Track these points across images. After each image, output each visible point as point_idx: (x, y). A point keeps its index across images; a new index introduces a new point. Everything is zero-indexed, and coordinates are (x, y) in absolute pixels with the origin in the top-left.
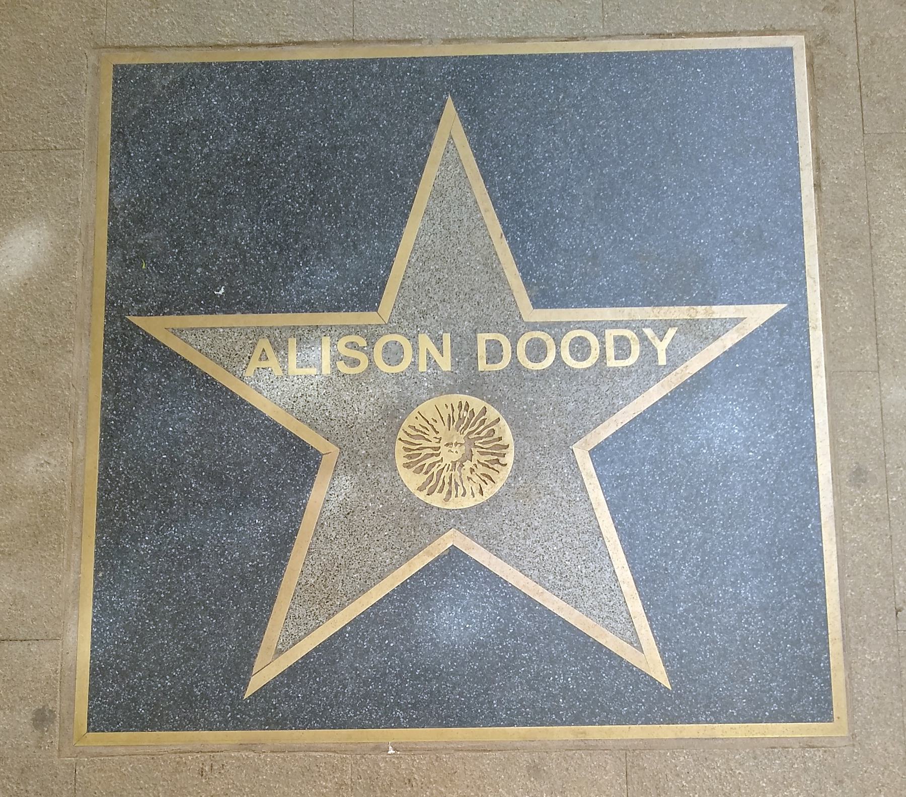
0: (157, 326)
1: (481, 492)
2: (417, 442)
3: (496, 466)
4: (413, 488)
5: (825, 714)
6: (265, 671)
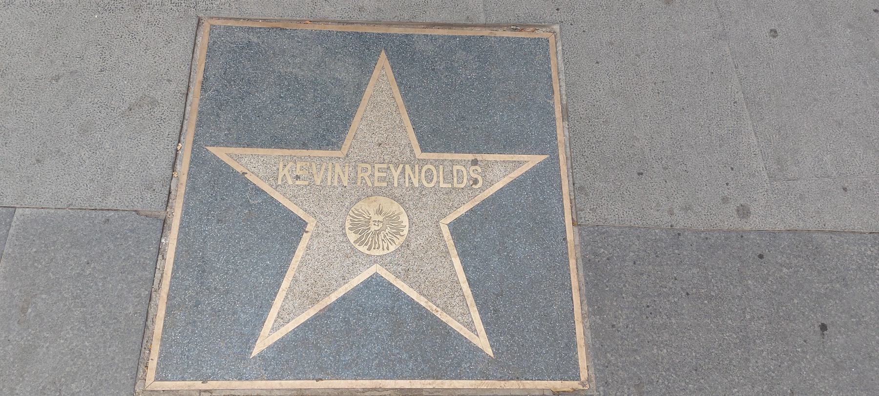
0: (221, 153)
6: (269, 336)
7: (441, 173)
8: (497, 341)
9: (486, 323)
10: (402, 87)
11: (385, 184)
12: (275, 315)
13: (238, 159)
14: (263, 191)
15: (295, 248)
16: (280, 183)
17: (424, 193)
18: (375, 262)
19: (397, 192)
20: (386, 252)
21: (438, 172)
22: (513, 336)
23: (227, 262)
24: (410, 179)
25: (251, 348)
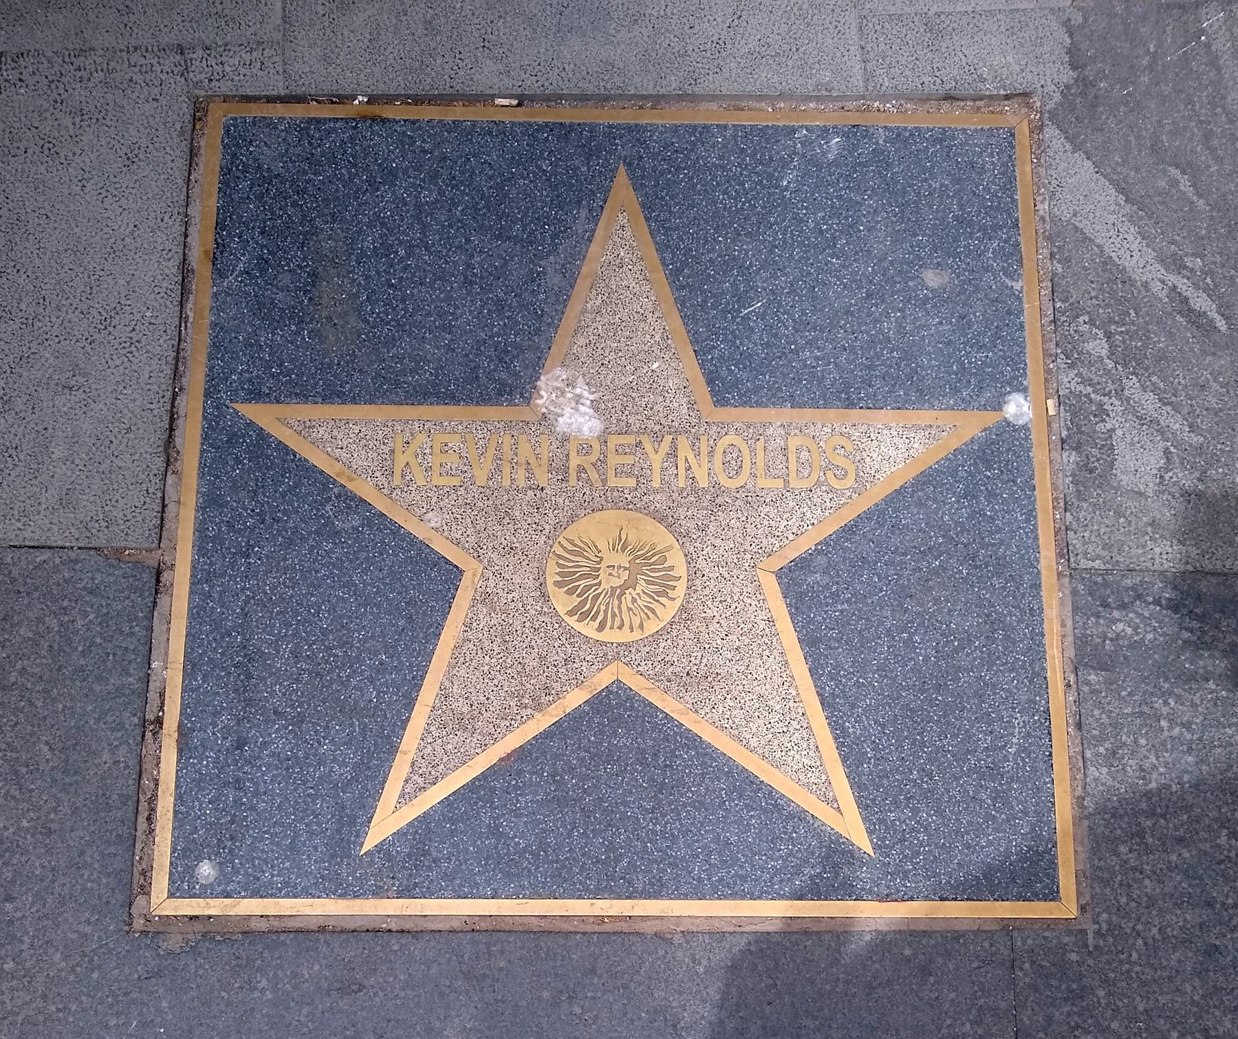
0: (262, 415)
1: (641, 626)
2: (573, 558)
3: (662, 600)
4: (562, 611)
5: (1052, 894)
6: (388, 821)
7: (760, 453)
8: (882, 821)
9: (857, 785)
10: (668, 256)
11: (632, 482)
12: (407, 769)
13: (305, 429)
14: (362, 501)
15: (440, 626)
16: (397, 480)
17: (719, 500)
18: (617, 657)
19: (660, 502)
20: (637, 635)
21: (753, 452)
22: (916, 811)
23: (295, 654)
24: (689, 469)
25: (360, 835)
